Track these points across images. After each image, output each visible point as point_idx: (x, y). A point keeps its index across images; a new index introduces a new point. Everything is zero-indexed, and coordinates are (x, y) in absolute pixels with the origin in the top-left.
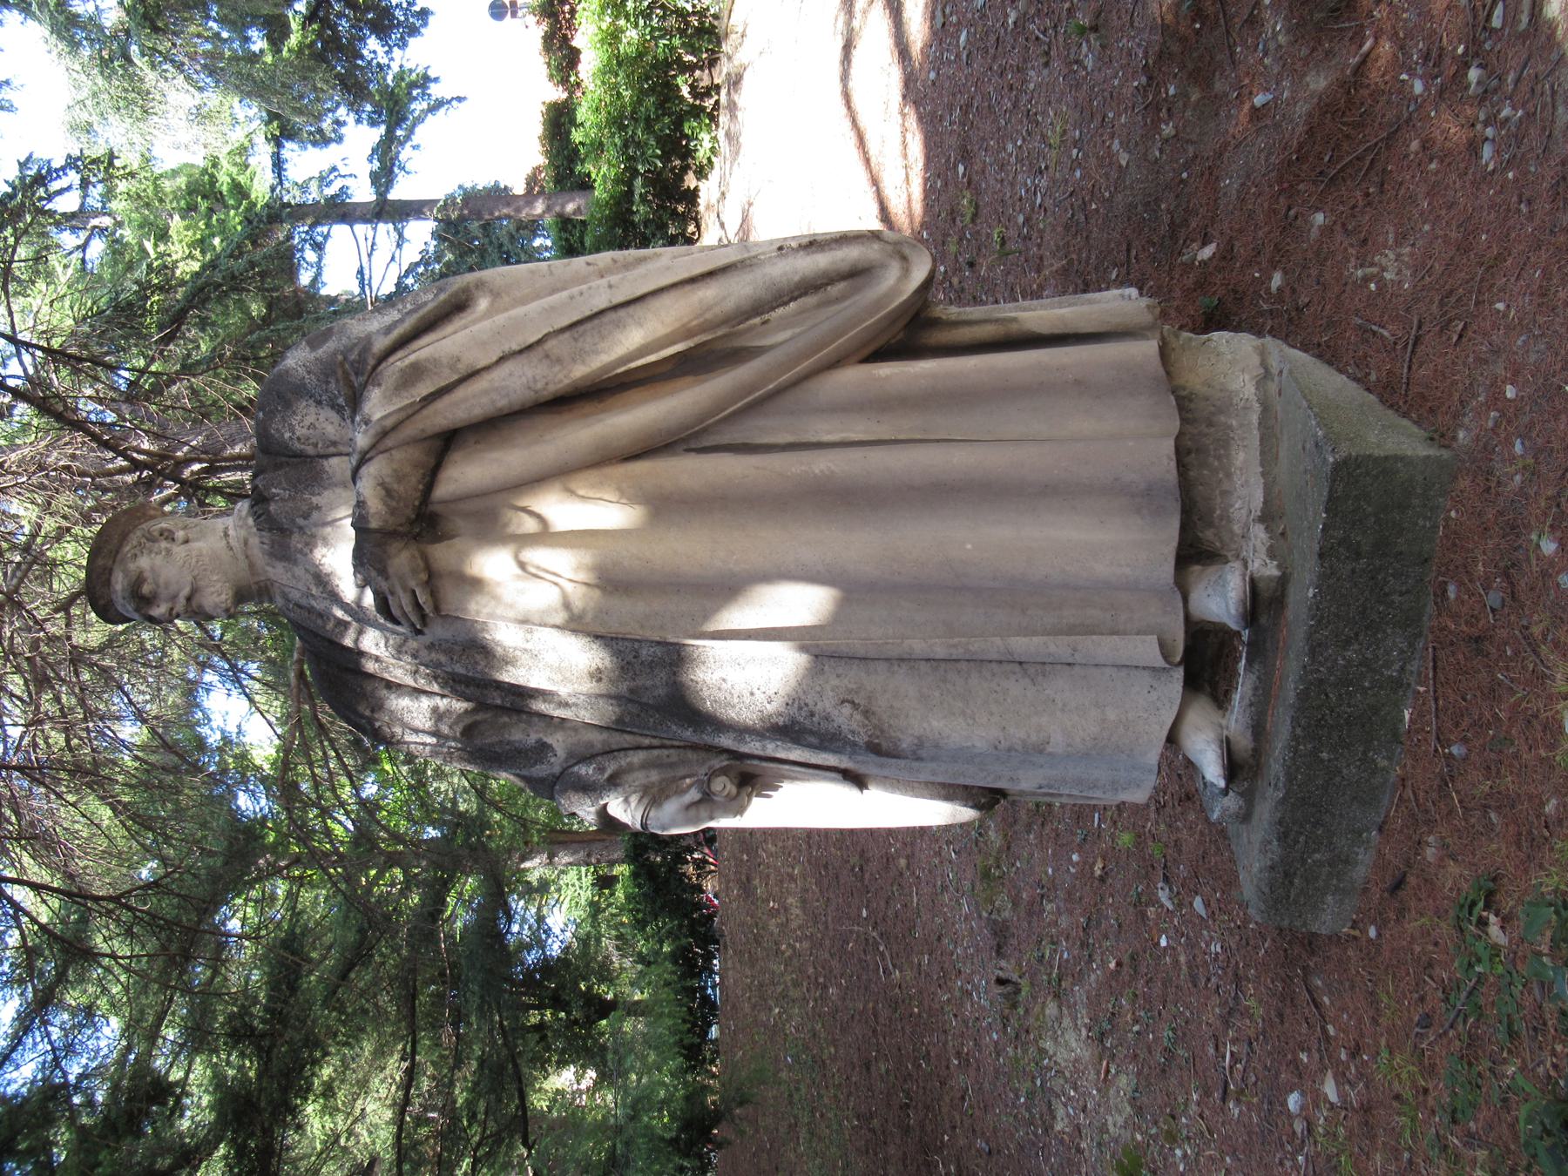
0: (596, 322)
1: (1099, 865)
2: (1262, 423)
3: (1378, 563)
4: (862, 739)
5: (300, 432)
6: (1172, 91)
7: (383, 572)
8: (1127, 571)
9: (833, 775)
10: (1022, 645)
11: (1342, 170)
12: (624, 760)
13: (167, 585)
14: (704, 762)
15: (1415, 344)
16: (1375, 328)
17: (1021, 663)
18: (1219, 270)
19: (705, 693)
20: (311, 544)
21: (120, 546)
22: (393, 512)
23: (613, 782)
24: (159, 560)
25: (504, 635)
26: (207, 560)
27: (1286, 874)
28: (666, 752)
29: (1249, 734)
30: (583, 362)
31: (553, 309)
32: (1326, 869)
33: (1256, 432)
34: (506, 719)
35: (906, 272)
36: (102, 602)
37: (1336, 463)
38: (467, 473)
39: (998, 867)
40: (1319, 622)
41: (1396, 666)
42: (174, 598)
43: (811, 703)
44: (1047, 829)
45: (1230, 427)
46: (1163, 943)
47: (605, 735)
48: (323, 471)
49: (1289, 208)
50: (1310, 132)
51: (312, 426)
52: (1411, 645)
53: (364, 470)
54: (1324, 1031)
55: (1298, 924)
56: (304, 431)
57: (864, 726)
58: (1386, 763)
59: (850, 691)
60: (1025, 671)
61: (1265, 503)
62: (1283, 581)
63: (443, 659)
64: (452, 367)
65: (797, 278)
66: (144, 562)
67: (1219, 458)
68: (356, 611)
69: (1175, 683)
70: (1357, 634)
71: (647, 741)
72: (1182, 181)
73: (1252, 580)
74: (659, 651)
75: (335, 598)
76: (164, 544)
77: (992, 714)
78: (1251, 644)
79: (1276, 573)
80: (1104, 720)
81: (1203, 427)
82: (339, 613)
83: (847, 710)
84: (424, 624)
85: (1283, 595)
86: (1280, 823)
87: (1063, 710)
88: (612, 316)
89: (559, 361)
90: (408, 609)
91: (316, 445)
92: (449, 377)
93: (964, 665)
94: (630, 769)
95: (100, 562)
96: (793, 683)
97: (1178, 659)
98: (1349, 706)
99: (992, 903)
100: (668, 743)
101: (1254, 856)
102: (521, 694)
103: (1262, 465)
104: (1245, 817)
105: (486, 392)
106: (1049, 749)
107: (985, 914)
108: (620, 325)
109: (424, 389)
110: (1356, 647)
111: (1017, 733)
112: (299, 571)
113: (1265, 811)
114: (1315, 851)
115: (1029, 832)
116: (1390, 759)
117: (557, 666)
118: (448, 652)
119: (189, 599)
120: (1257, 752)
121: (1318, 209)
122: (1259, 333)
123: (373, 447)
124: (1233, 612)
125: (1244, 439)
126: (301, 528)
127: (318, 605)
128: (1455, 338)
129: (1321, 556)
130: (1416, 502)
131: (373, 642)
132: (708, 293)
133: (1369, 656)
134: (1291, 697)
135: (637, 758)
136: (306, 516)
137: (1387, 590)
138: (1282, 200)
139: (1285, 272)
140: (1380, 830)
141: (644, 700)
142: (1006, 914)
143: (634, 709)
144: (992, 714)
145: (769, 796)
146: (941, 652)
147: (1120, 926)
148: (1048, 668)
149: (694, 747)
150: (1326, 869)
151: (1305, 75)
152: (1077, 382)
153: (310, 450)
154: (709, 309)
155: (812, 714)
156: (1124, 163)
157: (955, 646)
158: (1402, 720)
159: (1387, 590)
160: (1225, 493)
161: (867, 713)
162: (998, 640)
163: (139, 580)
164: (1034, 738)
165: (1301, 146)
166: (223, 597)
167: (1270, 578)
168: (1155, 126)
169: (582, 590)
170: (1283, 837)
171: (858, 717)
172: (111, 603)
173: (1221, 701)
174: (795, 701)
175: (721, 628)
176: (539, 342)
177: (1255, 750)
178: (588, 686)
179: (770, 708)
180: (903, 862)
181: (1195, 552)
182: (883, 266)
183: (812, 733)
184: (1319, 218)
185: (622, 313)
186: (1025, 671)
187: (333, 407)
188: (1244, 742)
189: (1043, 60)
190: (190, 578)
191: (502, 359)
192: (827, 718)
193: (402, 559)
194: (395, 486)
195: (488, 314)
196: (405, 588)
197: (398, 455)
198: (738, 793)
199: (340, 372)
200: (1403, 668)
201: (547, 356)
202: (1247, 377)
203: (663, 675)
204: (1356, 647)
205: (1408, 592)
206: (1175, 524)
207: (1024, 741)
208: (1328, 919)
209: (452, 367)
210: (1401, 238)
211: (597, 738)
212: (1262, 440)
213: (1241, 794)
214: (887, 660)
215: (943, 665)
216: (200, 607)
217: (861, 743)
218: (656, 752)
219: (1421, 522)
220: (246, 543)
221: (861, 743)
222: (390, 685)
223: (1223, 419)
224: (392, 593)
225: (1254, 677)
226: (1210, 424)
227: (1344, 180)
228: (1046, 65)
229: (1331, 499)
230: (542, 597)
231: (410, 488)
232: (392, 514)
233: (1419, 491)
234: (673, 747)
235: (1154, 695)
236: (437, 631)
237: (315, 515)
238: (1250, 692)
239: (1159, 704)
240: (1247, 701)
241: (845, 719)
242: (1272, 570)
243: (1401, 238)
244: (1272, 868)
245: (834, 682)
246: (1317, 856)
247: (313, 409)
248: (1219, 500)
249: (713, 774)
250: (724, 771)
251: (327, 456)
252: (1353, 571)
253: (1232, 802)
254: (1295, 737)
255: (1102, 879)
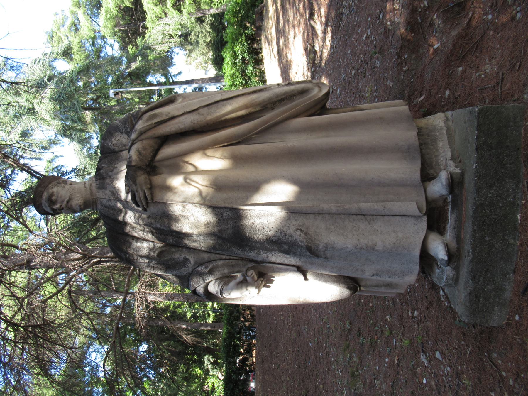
0: (216, 104)
1: (396, 359)
2: (448, 133)
3: (499, 151)
4: (304, 244)
5: (114, 142)
6: (406, 56)
7: (135, 182)
8: (403, 175)
9: (293, 268)
10: (365, 206)
11: (466, 53)
12: (215, 264)
13: (61, 197)
14: (245, 266)
15: (502, 81)
16: (487, 86)
17: (364, 215)
18: (426, 101)
19: (246, 230)
20: (112, 181)
21: (48, 185)
22: (140, 160)
23: (211, 272)
24: (60, 189)
25: (176, 209)
26: (76, 190)
27: (477, 297)
28: (231, 261)
29: (455, 241)
30: (211, 115)
31: (202, 100)
32: (493, 293)
33: (446, 136)
34: (173, 250)
35: (320, 90)
36: (38, 203)
37: (479, 110)
38: (168, 151)
39: (357, 371)
40: (479, 178)
41: (512, 196)
42: (63, 201)
43: (285, 230)
44: (376, 352)
45: (436, 135)
46: (424, 381)
47: (209, 255)
48: (120, 155)
49: (449, 71)
50: (454, 45)
51: (119, 140)
52: (517, 186)
53: (133, 147)
54: (501, 376)
55: (483, 321)
56: (116, 142)
57: (305, 238)
58: (512, 241)
59: (300, 226)
60: (366, 219)
61: (452, 156)
62: (462, 174)
63: (153, 221)
64: (166, 115)
65: (284, 92)
66: (55, 190)
67: (433, 145)
68: (125, 203)
69: (423, 224)
70: (494, 183)
71: (224, 257)
72: (412, 82)
73: (451, 174)
74: (229, 213)
75: (118, 199)
76: (63, 185)
77: (354, 235)
78: (453, 201)
79: (459, 171)
80: (397, 237)
81: (426, 137)
82: (119, 205)
83: (299, 232)
84: (147, 207)
85: (463, 180)
86: (471, 271)
87: (381, 234)
88: (222, 103)
89: (203, 114)
90: (142, 198)
91: (118, 147)
92: (165, 117)
93: (342, 216)
94: (217, 267)
95: (40, 189)
96: (279, 223)
97: (424, 212)
98: (495, 215)
99: (356, 386)
100: (232, 258)
101: (459, 299)
102: (181, 235)
103: (449, 145)
104: (456, 280)
105: (177, 123)
106: (377, 248)
107: (353, 391)
108: (224, 105)
109: (156, 120)
110: (495, 188)
111: (364, 242)
112: (107, 192)
113: (465, 271)
114: (488, 284)
115: (368, 355)
116: (514, 239)
117: (193, 219)
118: (155, 219)
119: (68, 202)
120: (459, 249)
121: (459, 67)
122: (444, 112)
123: (137, 138)
124: (444, 183)
125: (441, 138)
126: (110, 176)
127: (112, 204)
128: (517, 68)
129: (477, 149)
130: (511, 124)
131: (130, 217)
132: (254, 96)
133: (501, 192)
134: (471, 213)
135: (220, 263)
136: (112, 171)
137: (504, 162)
138: (446, 70)
139: (450, 89)
140: (514, 272)
141: (224, 236)
142: (361, 390)
143: (220, 241)
144: (354, 235)
145: (269, 287)
146: (334, 209)
147: (406, 382)
148: (375, 217)
149: (242, 259)
150: (493, 293)
151: (450, 32)
152: (381, 118)
153: (117, 149)
154: (254, 100)
155: (285, 235)
156: (391, 86)
157: (339, 207)
158: (517, 221)
159: (504, 162)
160: (436, 156)
161: (306, 234)
162: (355, 205)
163: (52, 195)
164: (370, 243)
165: (451, 51)
166: (80, 201)
167: (457, 173)
168: (401, 70)
169: (206, 188)
170: (473, 278)
171: (303, 235)
172: (41, 204)
173: (441, 232)
174: (280, 230)
175: (253, 203)
176: (197, 109)
177: (458, 248)
178: (203, 229)
179: (270, 234)
180: (321, 386)
181: (427, 176)
182: (312, 89)
183: (286, 243)
184: (461, 69)
185: (225, 102)
186: (366, 219)
187: (126, 133)
188: (453, 245)
189: (363, 75)
190: (69, 194)
191: (183, 114)
192: (291, 236)
193: (142, 178)
194: (143, 152)
195: (181, 102)
196: (142, 189)
197: (144, 142)
198: (257, 280)
199: (130, 120)
200: (514, 197)
201: (199, 113)
202: (440, 120)
203: (231, 223)
204: (495, 188)
205: (513, 163)
206: (419, 163)
207: (366, 245)
208: (497, 318)
209: (166, 115)
210: (491, 58)
211: (206, 256)
212: (448, 138)
213: (454, 268)
214: (314, 214)
215: (335, 216)
216: (71, 206)
217: (304, 246)
218: (227, 261)
219: (514, 133)
220: (91, 185)
221: (304, 246)
222: (134, 237)
223: (433, 133)
224: (137, 191)
225: (455, 216)
226: (429, 136)
227: (467, 56)
228: (365, 77)
229: (478, 125)
230: (191, 191)
231: (148, 153)
232: (140, 161)
233: (512, 120)
234: (234, 259)
235: (416, 227)
236: (152, 209)
237: (115, 170)
238: (454, 223)
239: (418, 231)
240: (452, 227)
241: (298, 236)
242: (458, 171)
243: (491, 58)
244: (470, 293)
245: (294, 222)
246: (489, 287)
247: (119, 135)
248: (434, 159)
249: (248, 270)
250: (252, 268)
251: (122, 151)
252: (490, 155)
253: (449, 271)
254: (474, 231)
255: (398, 365)
